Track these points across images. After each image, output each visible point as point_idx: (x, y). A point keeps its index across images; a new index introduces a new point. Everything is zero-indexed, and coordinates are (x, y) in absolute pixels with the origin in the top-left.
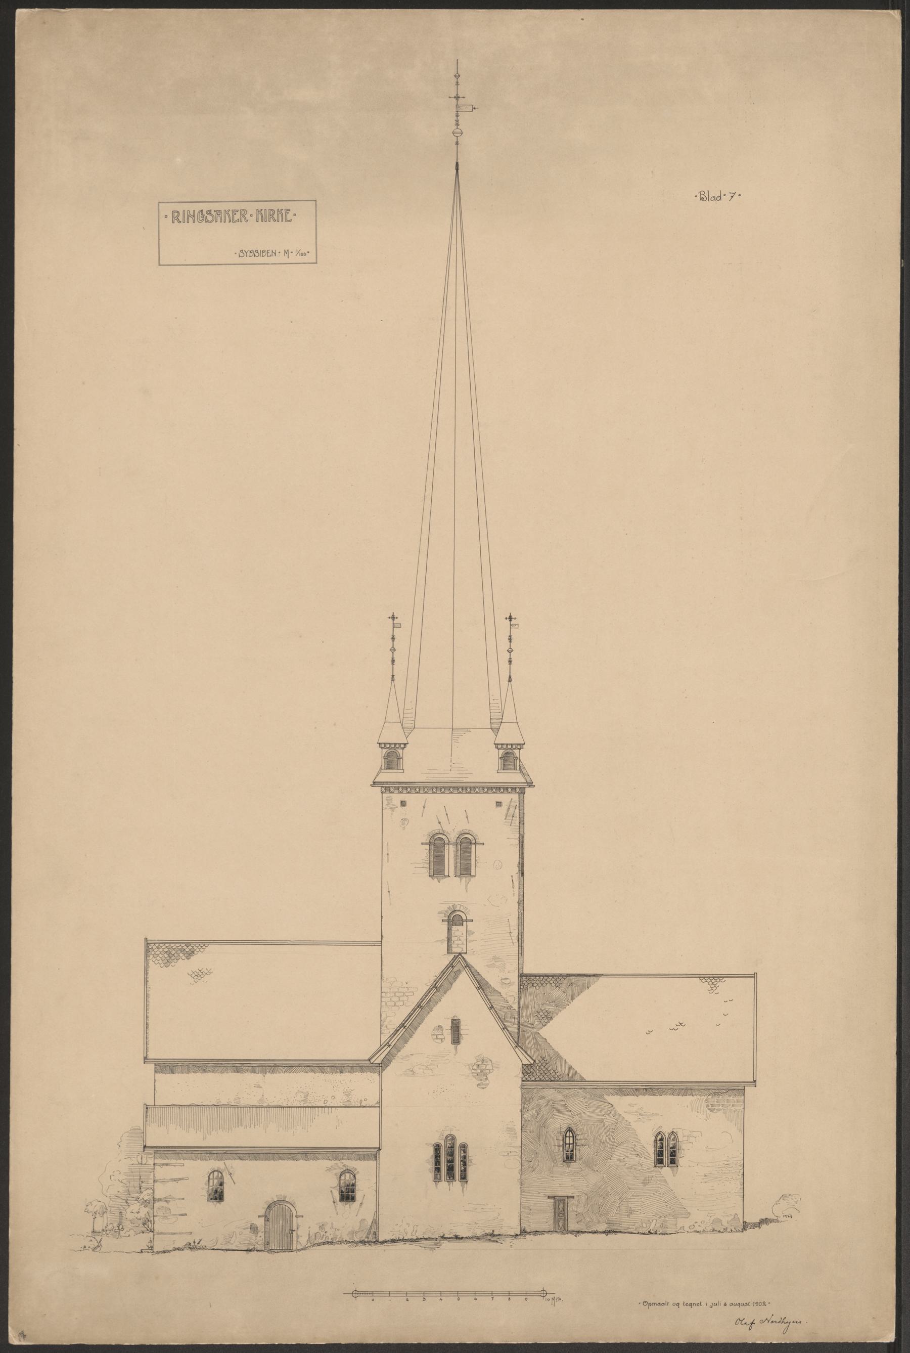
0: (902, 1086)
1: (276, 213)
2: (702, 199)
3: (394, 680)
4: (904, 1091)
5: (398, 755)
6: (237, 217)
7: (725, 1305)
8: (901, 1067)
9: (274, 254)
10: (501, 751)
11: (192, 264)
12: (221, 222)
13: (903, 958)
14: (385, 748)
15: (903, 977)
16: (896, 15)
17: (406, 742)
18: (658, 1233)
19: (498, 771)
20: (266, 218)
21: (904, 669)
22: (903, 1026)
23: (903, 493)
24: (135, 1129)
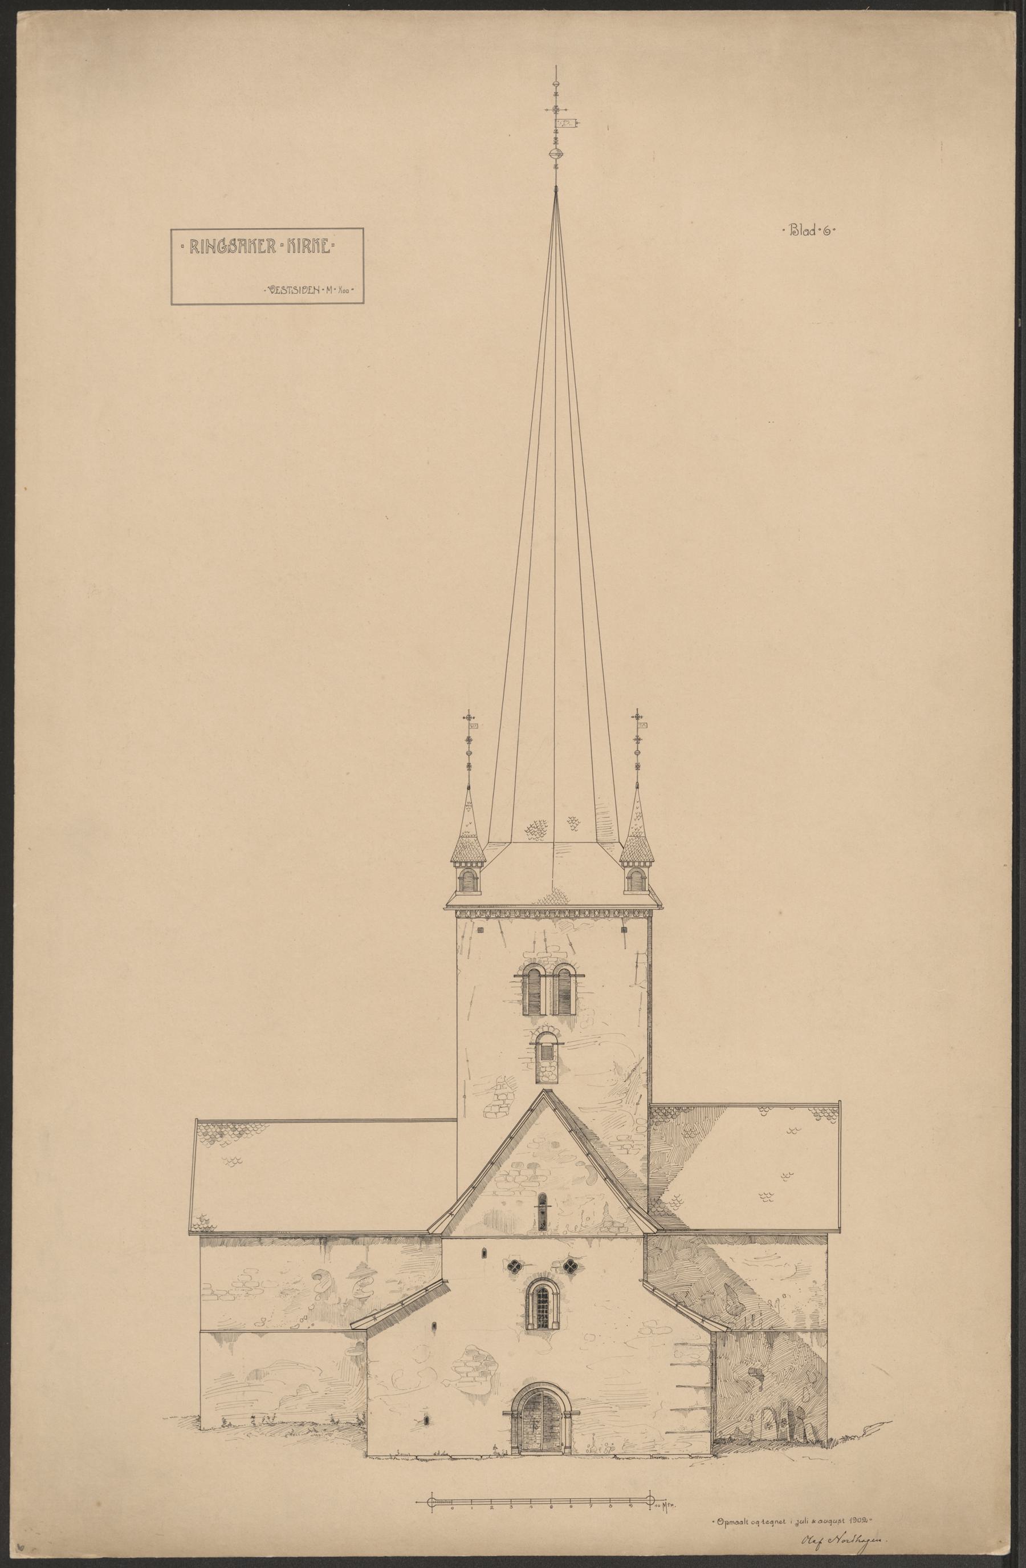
0: (1019, 1279)
1: (312, 242)
2: (793, 233)
5: (475, 876)
7: (814, 1522)
9: (316, 291)
11: (271, 305)
13: (1020, 1130)
15: (1020, 1152)
21: (1021, 794)
22: (1020, 1209)
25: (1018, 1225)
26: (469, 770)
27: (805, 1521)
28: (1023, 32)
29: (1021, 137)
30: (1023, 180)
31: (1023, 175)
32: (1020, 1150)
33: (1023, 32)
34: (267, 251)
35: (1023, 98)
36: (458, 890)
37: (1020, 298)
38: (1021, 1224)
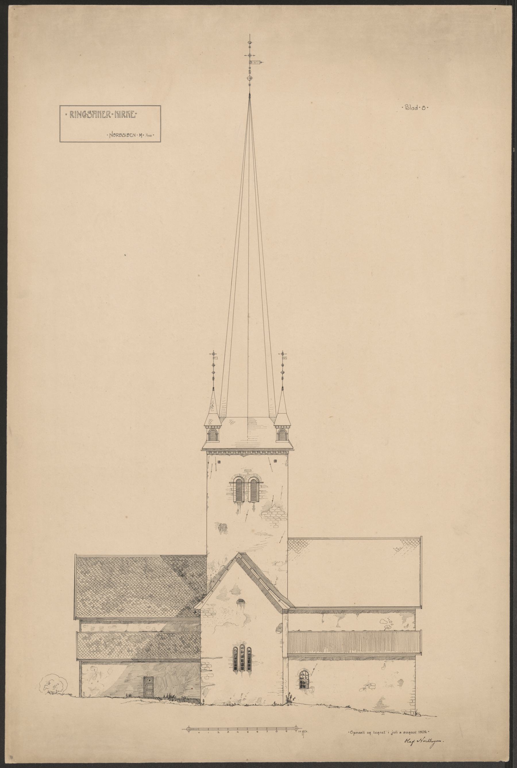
0: (513, 619)
3: (214, 390)
4: (514, 622)
6: (105, 115)
7: (400, 733)
8: (513, 608)
9: (134, 136)
10: (278, 430)
12: (130, 117)
13: (514, 546)
14: (209, 428)
15: (514, 556)
17: (290, 425)
18: (132, 696)
19: (277, 441)
20: (120, 116)
21: (514, 381)
25: (513, 592)
26: (213, 380)
27: (396, 732)
28: (516, 7)
29: (515, 59)
30: (515, 80)
31: (515, 77)
32: (514, 555)
33: (516, 7)
34: (106, 117)
35: (515, 40)
36: (208, 440)
37: (514, 138)
38: (514, 592)
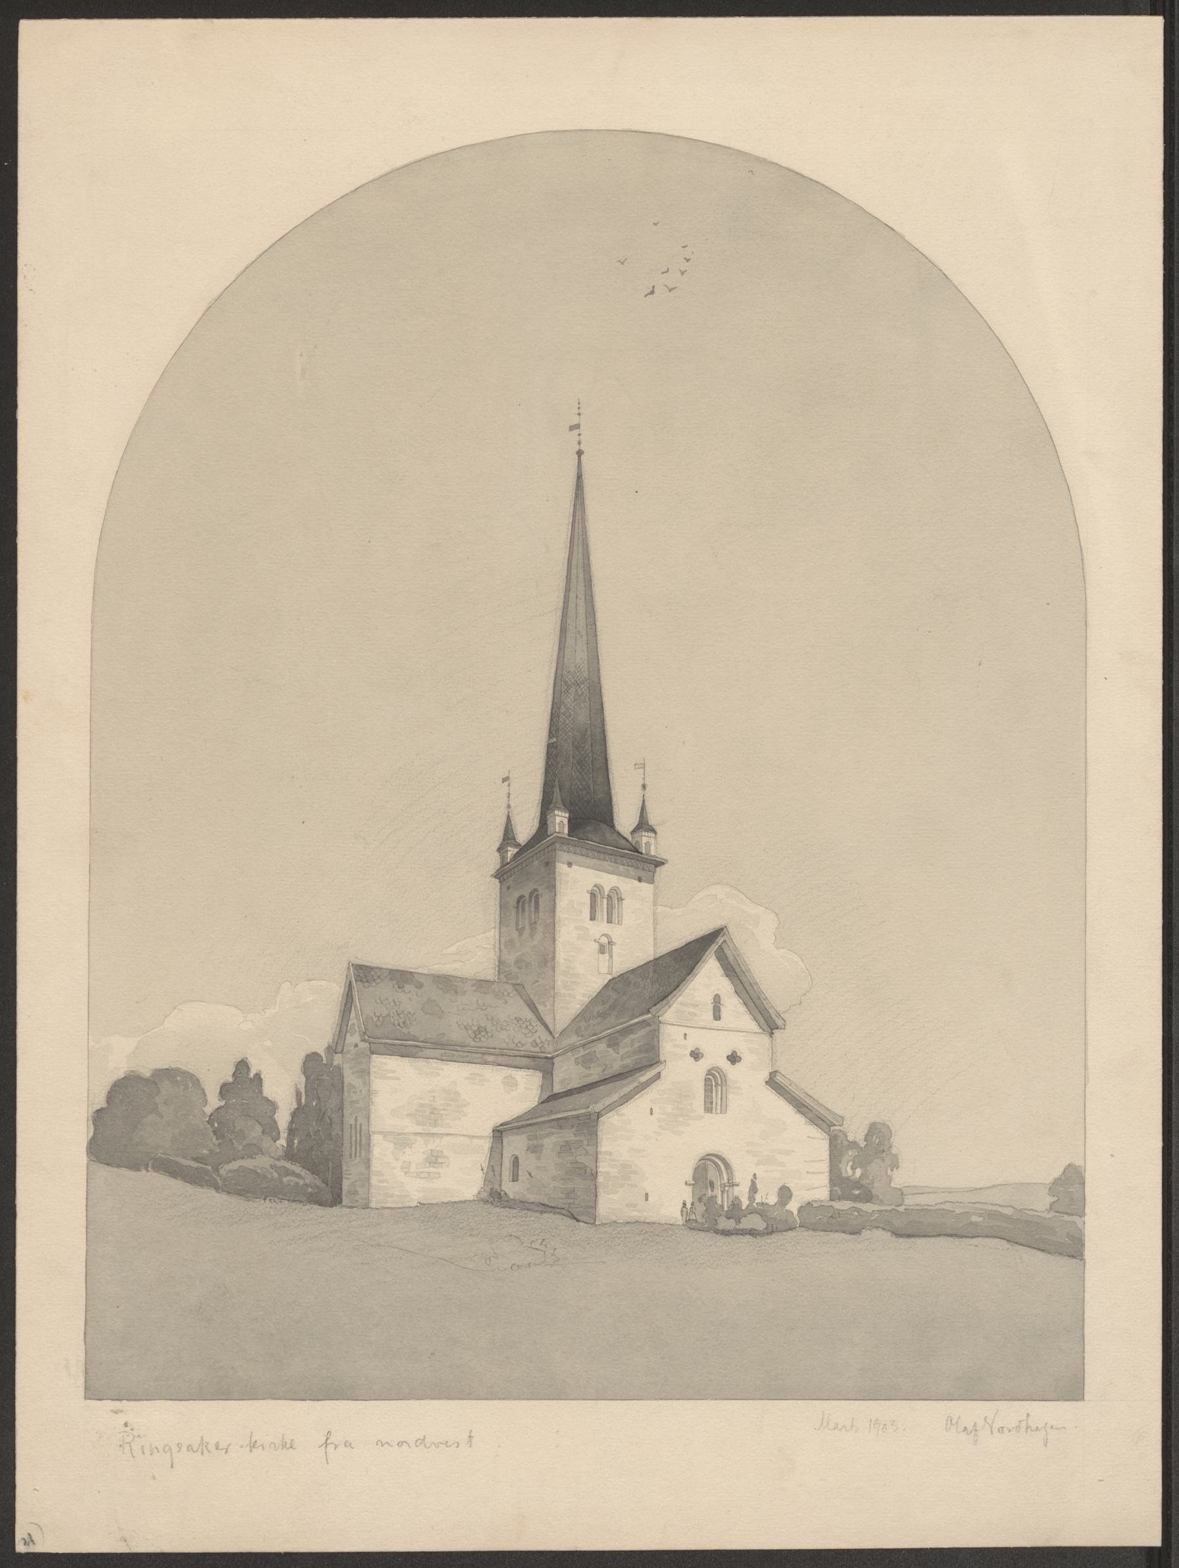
4: (1175, 1328)
15: (1174, 1120)
16: (1155, 25)
23: (1173, 241)
24: (575, 1019)
